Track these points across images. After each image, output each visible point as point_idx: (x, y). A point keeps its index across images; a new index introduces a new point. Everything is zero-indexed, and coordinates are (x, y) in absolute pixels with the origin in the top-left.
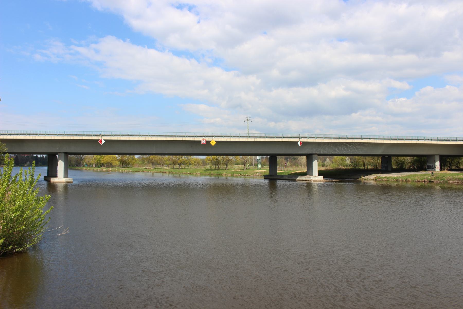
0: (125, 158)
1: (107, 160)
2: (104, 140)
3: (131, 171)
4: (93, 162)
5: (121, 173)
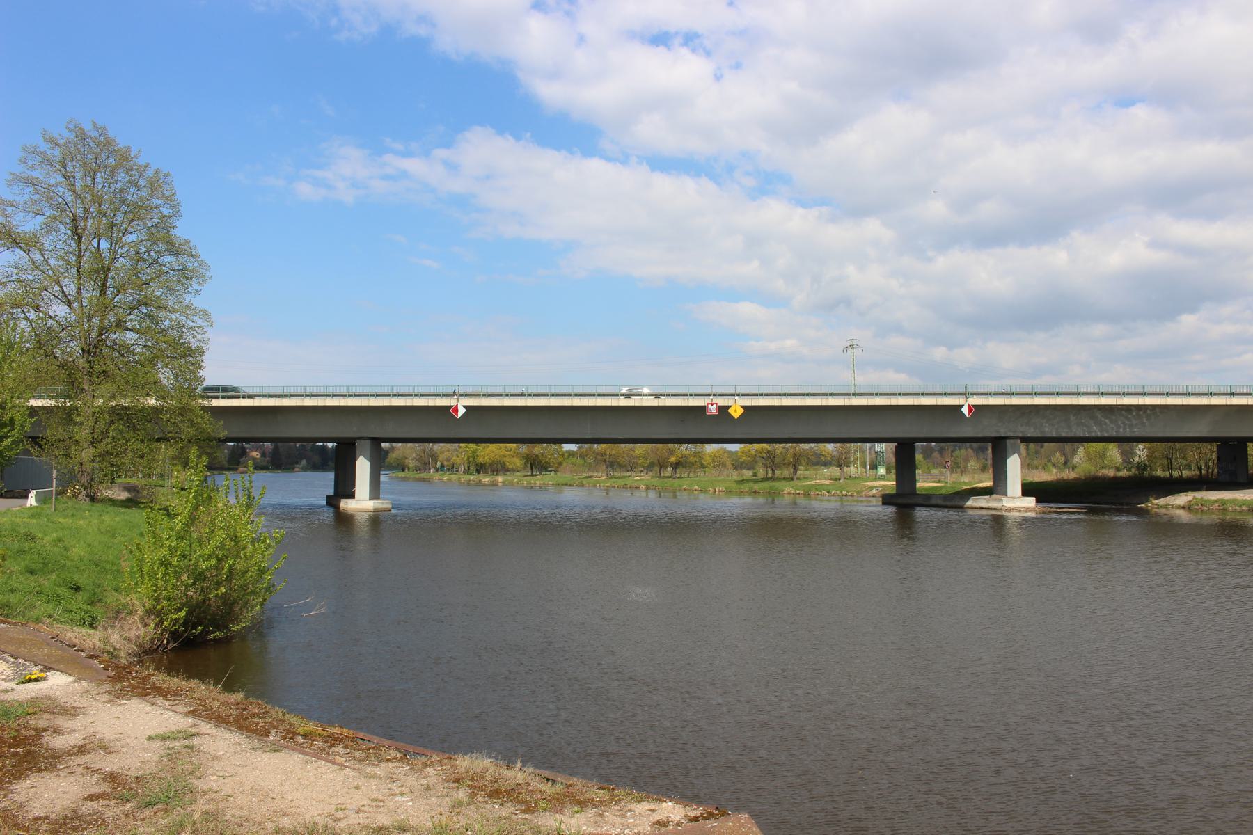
0: (538, 449)
1: (492, 455)
2: (465, 407)
3: (550, 483)
4: (458, 461)
5: (526, 487)
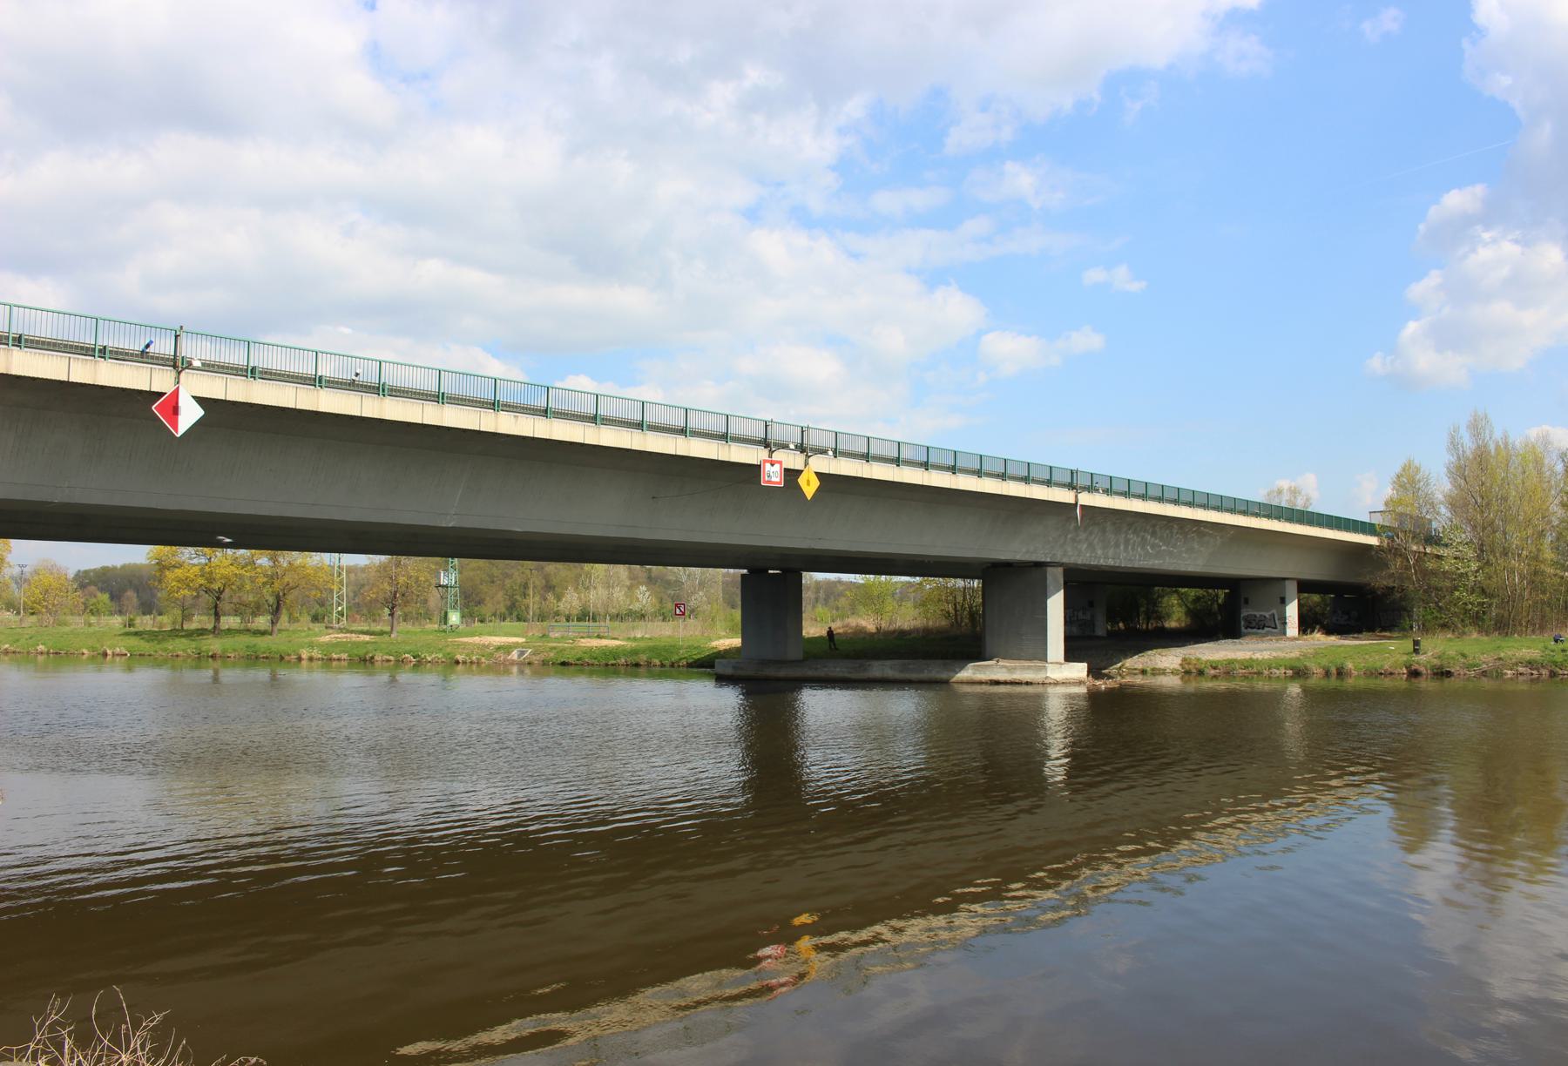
2: (201, 401)
